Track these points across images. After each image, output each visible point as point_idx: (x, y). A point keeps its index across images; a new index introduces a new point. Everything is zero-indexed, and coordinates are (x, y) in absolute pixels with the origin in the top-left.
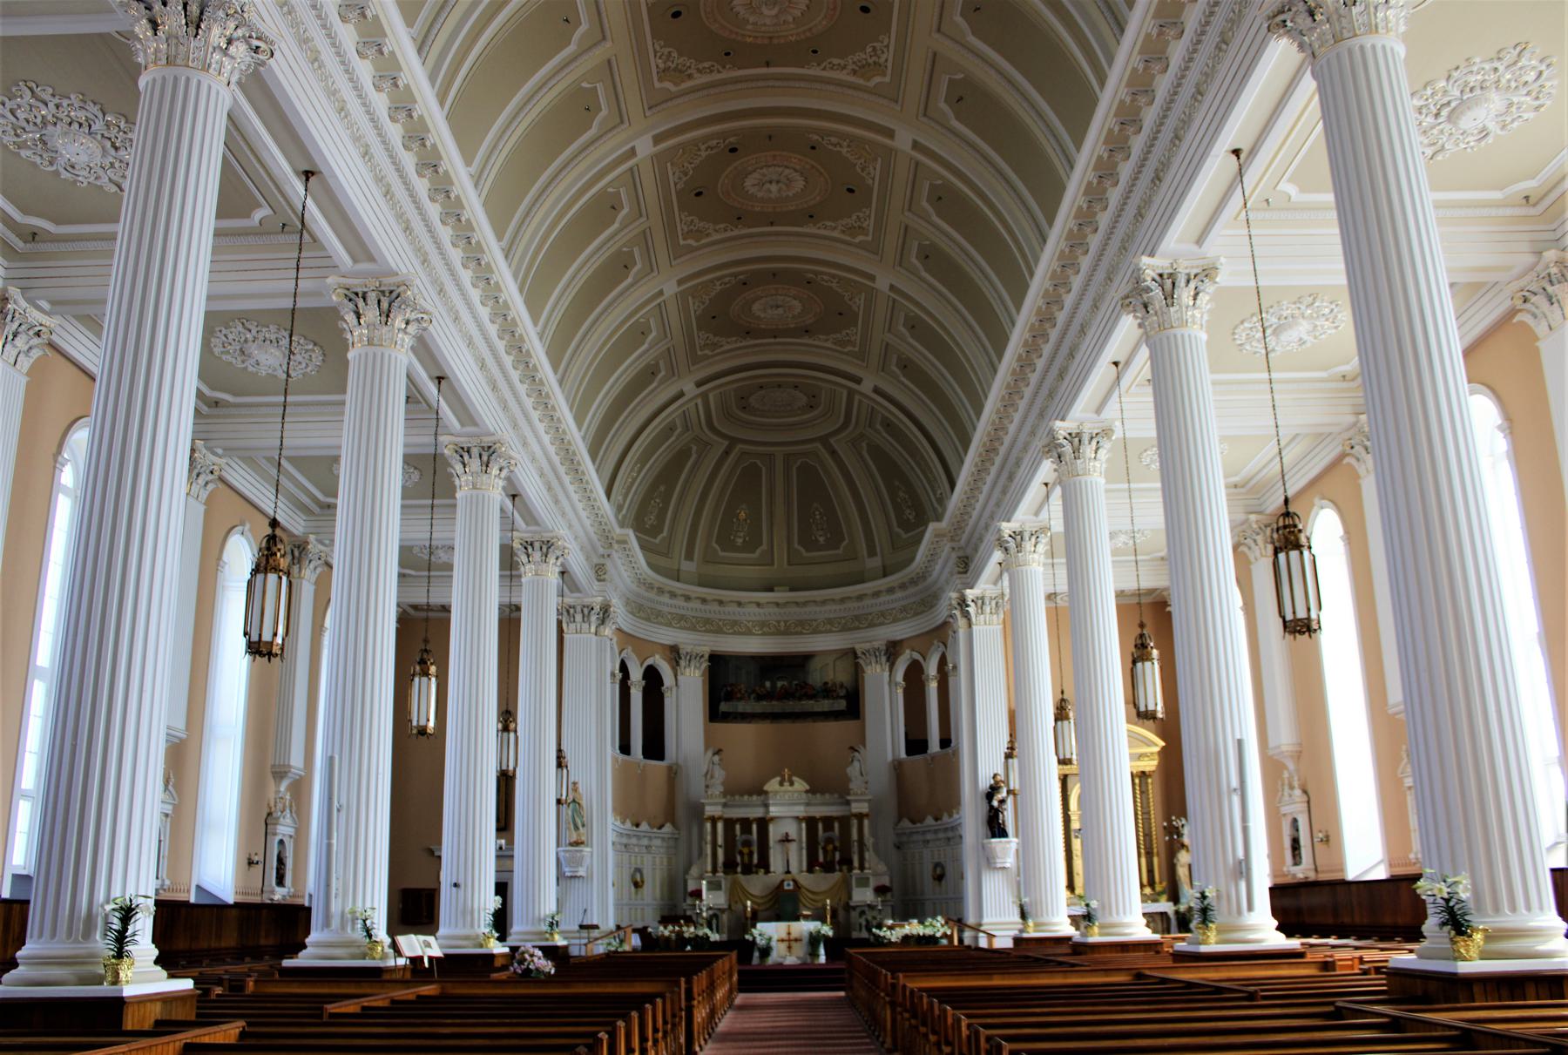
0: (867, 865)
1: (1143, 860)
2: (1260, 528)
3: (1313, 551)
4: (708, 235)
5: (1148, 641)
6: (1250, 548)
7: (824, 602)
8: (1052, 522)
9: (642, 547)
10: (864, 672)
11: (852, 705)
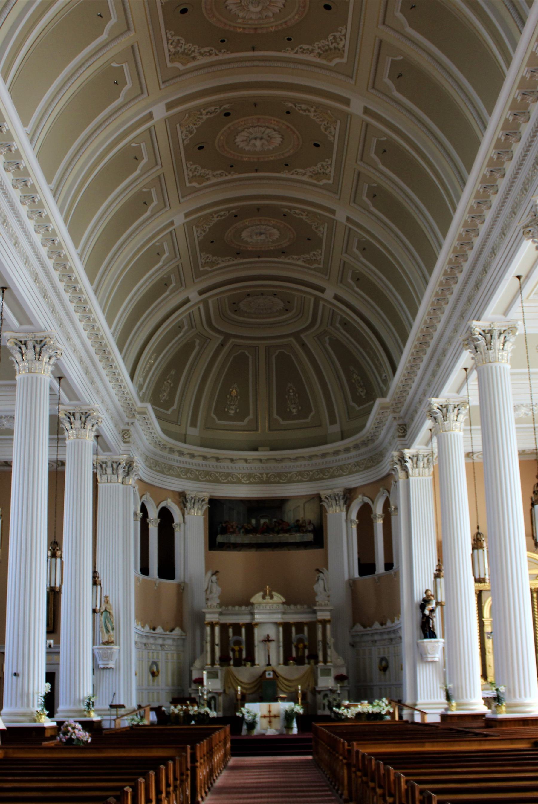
0: (329, 659)
9: (158, 417)
10: (327, 512)
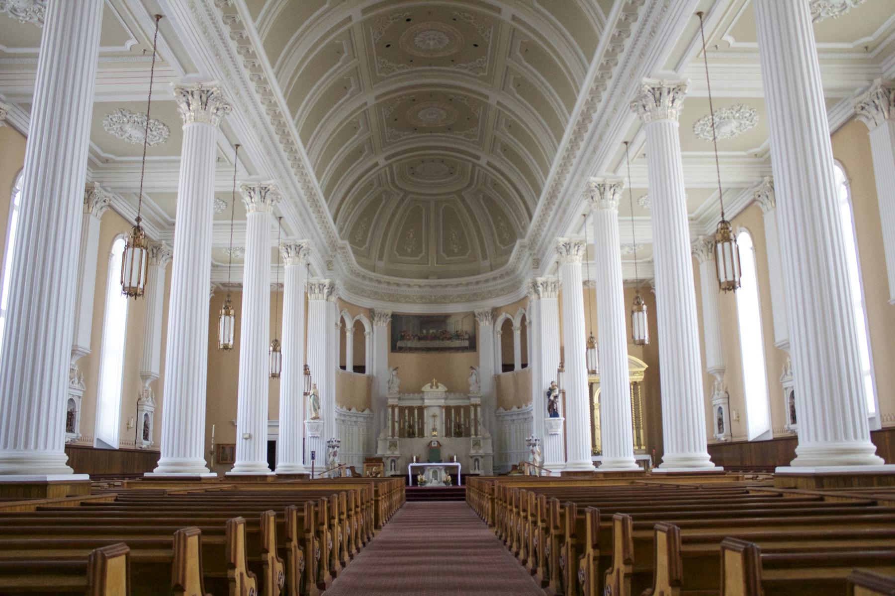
0: (479, 433)
1: (635, 431)
3: (737, 243)
4: (393, 71)
5: (641, 300)
6: (699, 255)
7: (457, 285)
8: (587, 238)
9: (354, 253)
10: (479, 325)
11: (473, 345)
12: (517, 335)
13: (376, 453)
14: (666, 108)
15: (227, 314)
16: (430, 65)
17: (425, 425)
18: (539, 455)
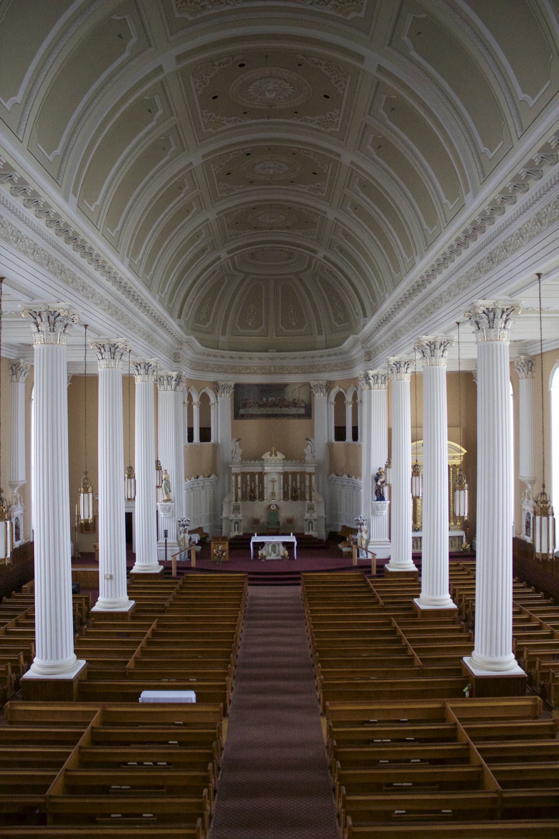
0: (313, 498)
2: (526, 362)
3: (555, 516)
7: (294, 358)
10: (314, 395)
11: (308, 413)
12: (349, 408)
13: (222, 515)
14: (499, 330)
15: (86, 491)
16: (270, 184)
17: (265, 490)
18: (366, 533)
